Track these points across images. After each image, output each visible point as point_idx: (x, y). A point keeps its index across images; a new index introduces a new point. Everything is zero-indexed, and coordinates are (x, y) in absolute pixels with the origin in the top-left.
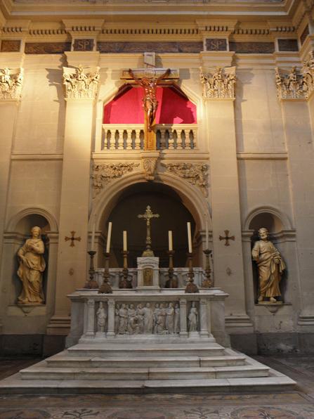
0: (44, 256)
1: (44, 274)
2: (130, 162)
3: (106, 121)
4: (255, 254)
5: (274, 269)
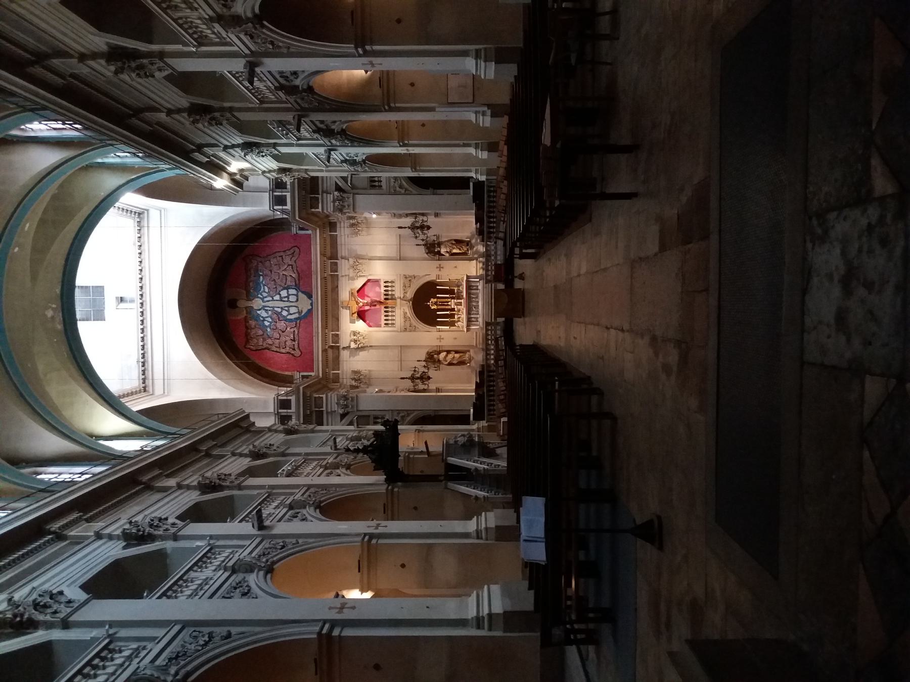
0: (448, 352)
1: (457, 352)
3: (379, 326)
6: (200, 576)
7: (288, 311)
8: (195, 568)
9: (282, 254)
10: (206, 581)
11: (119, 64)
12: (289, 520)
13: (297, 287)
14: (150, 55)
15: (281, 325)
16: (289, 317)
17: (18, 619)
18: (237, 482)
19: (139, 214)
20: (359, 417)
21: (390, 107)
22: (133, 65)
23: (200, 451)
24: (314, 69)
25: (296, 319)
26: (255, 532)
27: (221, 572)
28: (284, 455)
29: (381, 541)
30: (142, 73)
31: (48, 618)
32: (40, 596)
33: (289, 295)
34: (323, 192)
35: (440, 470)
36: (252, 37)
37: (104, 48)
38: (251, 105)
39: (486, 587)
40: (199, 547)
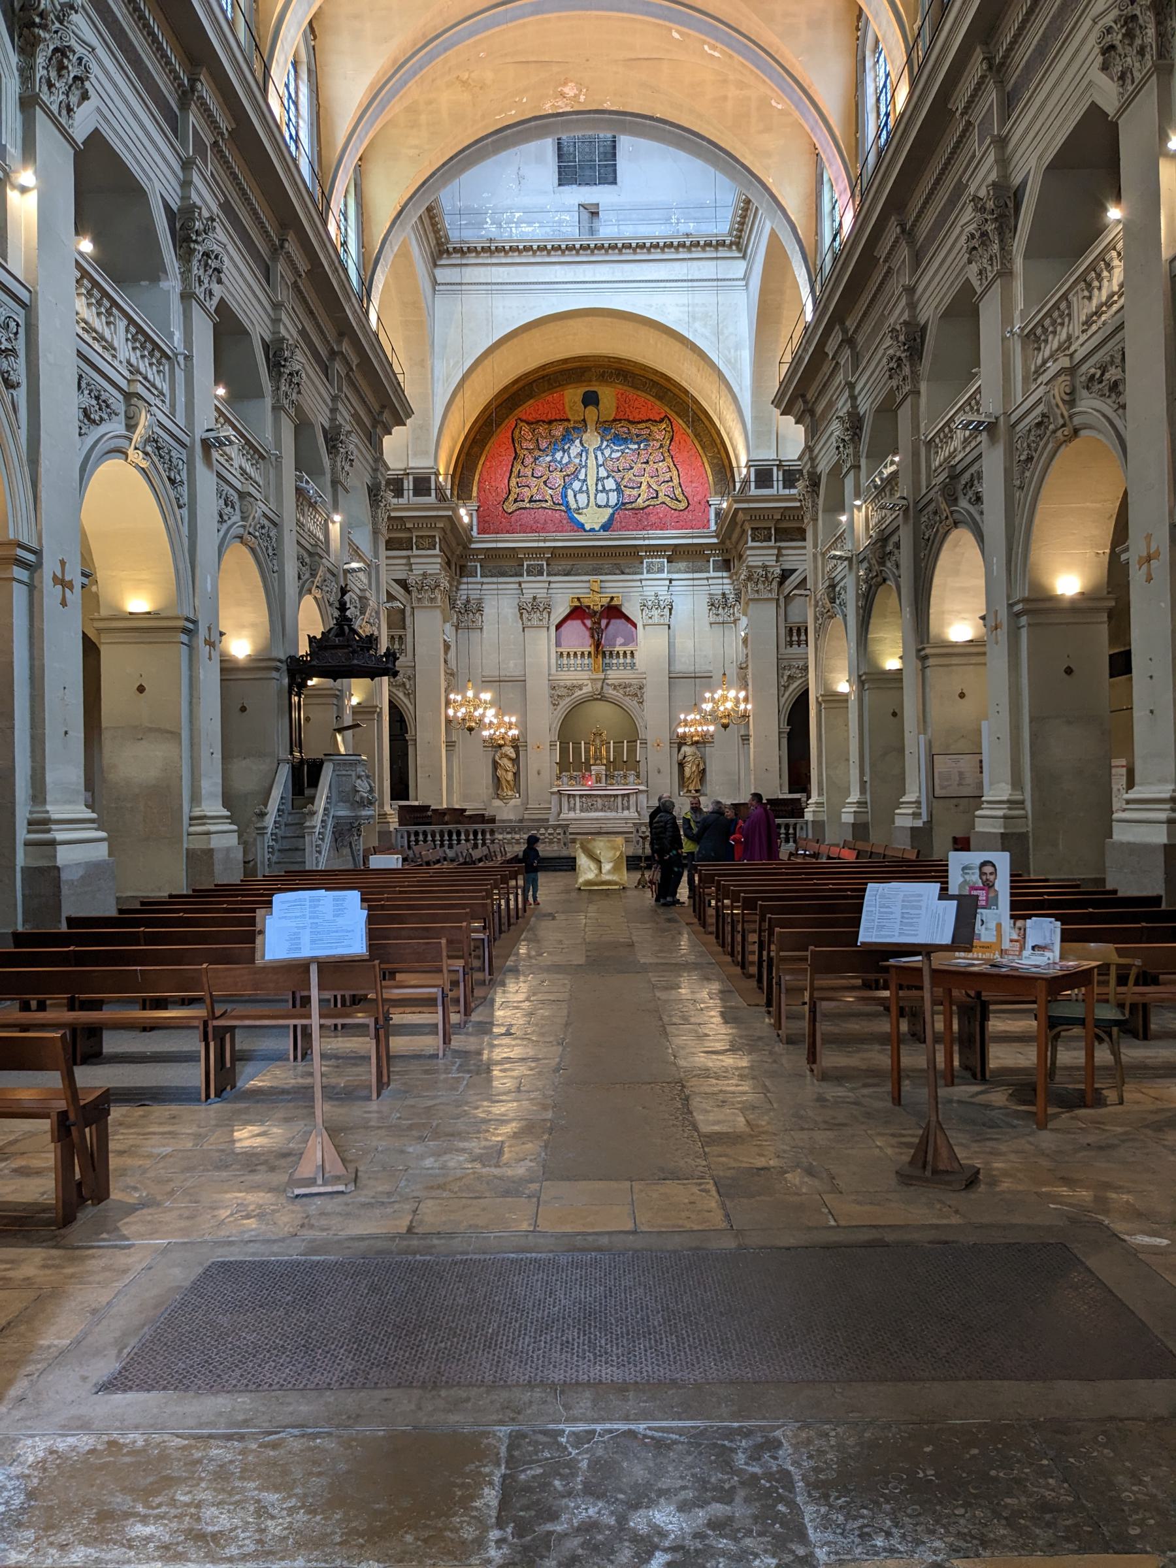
0: (515, 761)
1: (516, 775)
2: (580, 682)
4: (681, 757)
5: (694, 768)
6: (119, 335)
7: (581, 491)
8: (133, 330)
9: (676, 481)
10: (109, 347)
11: (990, 205)
12: (220, 493)
13: (621, 506)
14: (1005, 250)
15: (557, 479)
16: (570, 493)
17: (37, 20)
18: (285, 402)
19: (738, 244)
20: (403, 611)
21: (1018, 615)
22: (990, 227)
23: (340, 342)
24: (985, 530)
25: (568, 506)
26: (199, 434)
27: (126, 374)
28: (335, 483)
29: (19, 595)
30: (975, 243)
31: (40, 72)
32: (80, 59)
33: (607, 492)
34: (779, 548)
35: (312, 752)
36: (1039, 425)
37: (819, 470)
38: (922, 425)
39: (103, 834)
40: (171, 336)
